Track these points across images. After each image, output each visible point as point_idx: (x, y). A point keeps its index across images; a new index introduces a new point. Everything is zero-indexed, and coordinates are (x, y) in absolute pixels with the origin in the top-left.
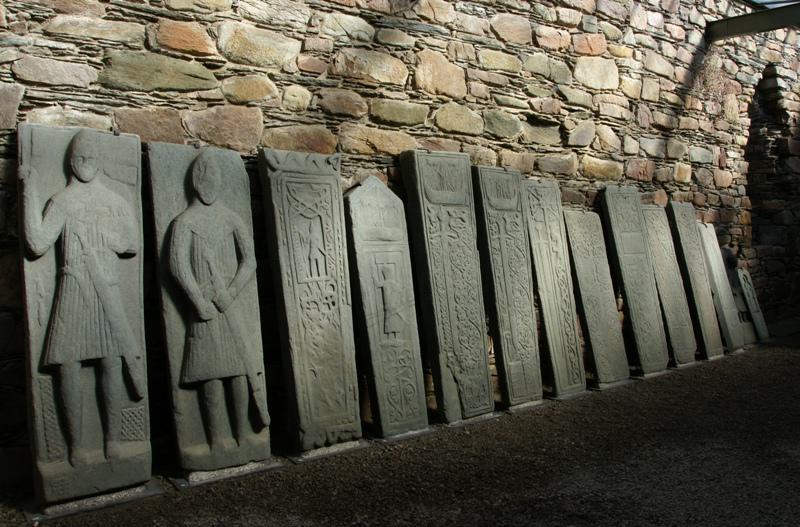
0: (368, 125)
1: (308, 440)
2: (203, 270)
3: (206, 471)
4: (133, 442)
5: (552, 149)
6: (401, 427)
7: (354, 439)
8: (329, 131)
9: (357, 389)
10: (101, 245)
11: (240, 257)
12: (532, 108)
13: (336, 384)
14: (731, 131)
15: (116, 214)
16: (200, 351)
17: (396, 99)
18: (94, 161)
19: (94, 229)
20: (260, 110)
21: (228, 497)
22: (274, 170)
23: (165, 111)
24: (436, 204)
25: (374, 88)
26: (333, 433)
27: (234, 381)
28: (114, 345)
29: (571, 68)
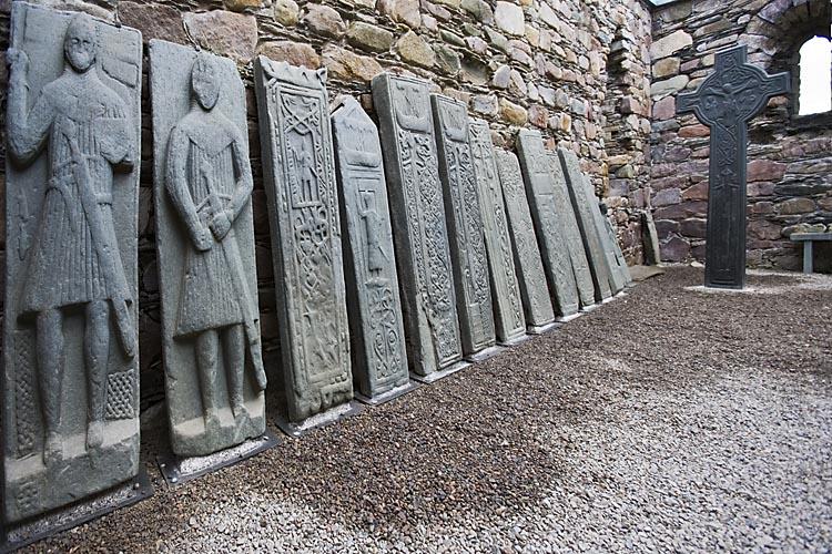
0: (346, 48)
1: (303, 405)
2: (199, 188)
3: (200, 456)
4: (120, 421)
5: (481, 89)
6: (387, 383)
7: (347, 401)
8: (314, 50)
9: (348, 337)
10: (93, 151)
11: (237, 174)
12: (467, 45)
13: (329, 333)
14: (594, 86)
15: (112, 114)
16: (197, 292)
17: (368, 22)
18: (90, 48)
19: (87, 130)
20: (255, 19)
21: (720, 367)
22: (269, 78)
23: (168, 9)
24: (407, 130)
25: (351, 9)
26: (327, 395)
27: (230, 333)
28: (101, 285)
29: (493, 11)
